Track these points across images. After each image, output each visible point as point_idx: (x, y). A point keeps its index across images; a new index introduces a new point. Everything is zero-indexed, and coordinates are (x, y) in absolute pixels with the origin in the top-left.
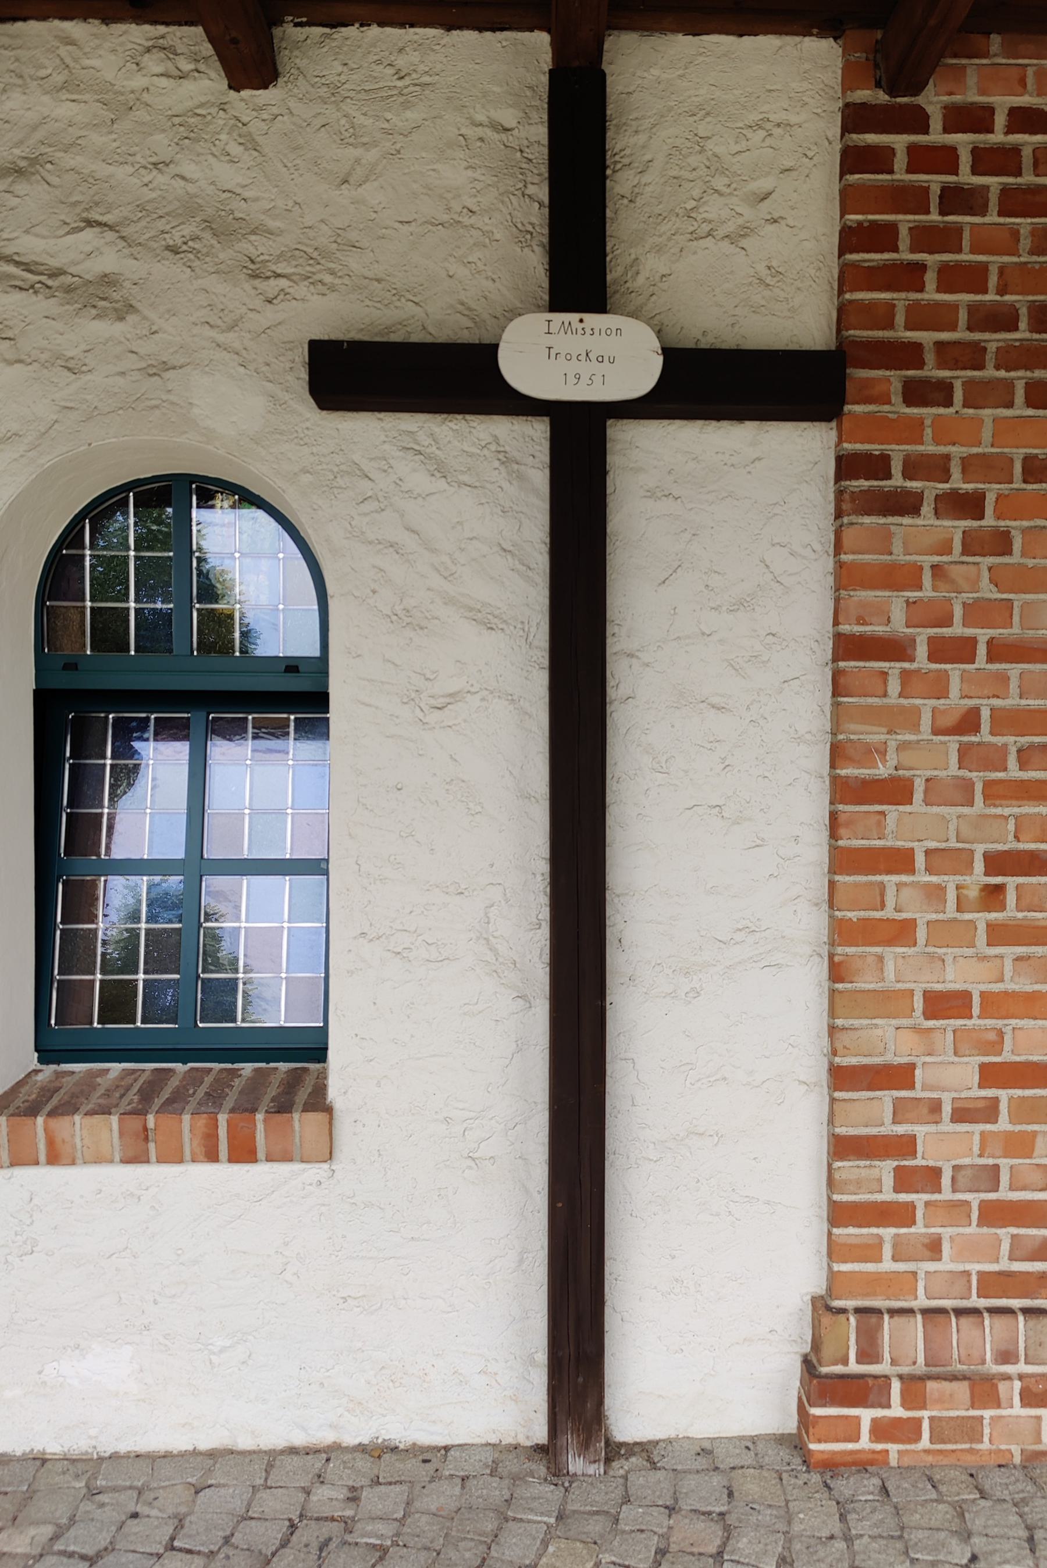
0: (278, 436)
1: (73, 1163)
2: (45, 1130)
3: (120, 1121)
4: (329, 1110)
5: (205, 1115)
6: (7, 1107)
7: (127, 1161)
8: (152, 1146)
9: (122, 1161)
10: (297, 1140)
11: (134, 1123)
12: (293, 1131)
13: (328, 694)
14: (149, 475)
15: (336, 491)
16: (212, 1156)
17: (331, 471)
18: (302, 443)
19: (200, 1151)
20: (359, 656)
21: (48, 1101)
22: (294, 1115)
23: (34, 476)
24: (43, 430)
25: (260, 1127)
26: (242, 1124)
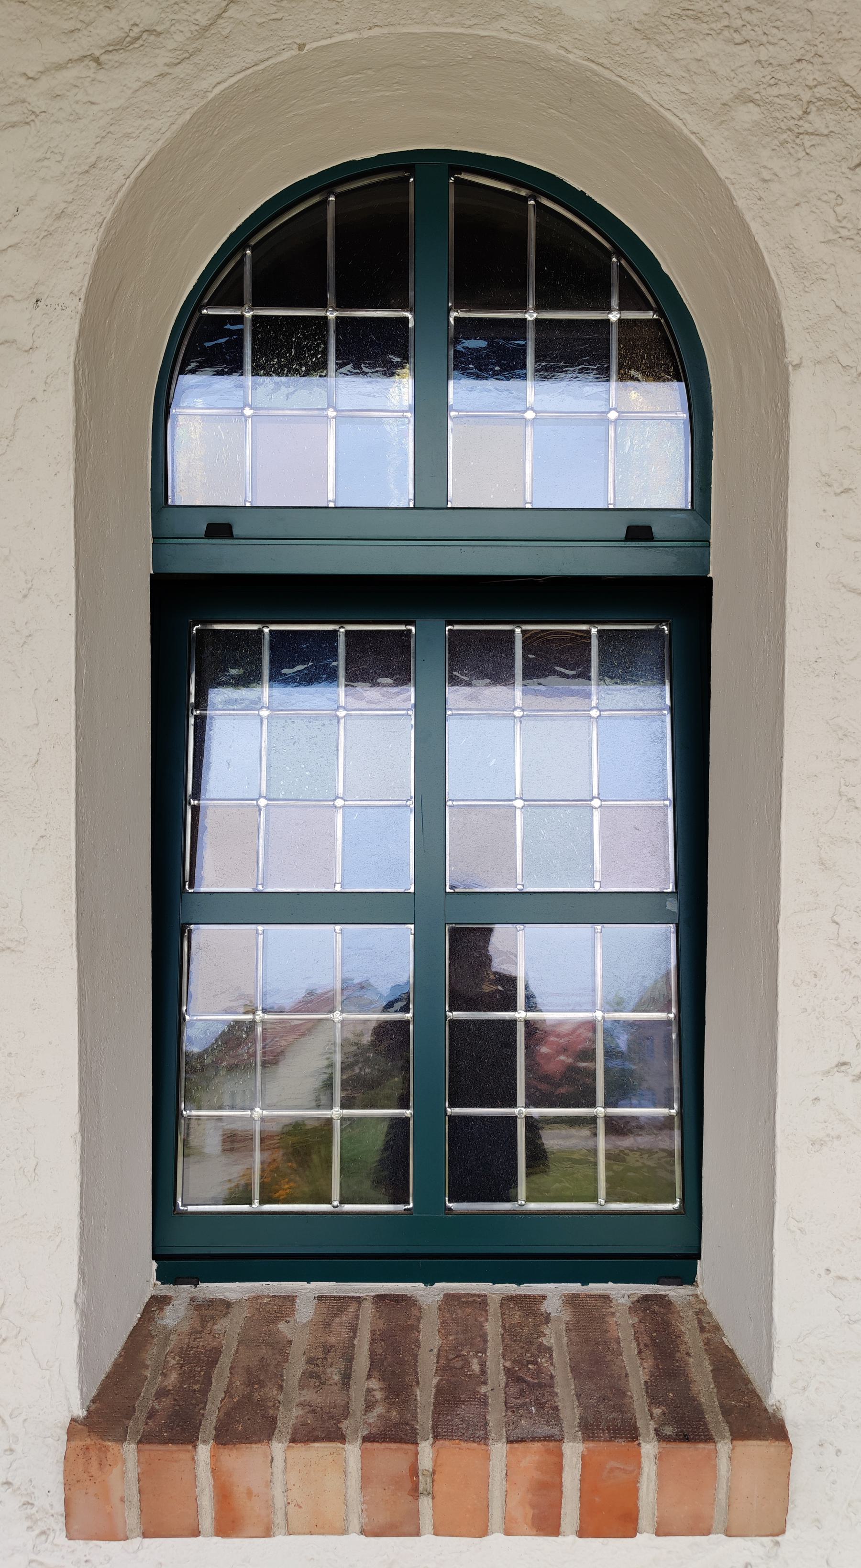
0: (689, 24)
1: (268, 1533)
2: (213, 1471)
3: (364, 1455)
4: (775, 1430)
5: (537, 1445)
6: (129, 1413)
7: (373, 1531)
8: (425, 1504)
9: (363, 1532)
10: (722, 1495)
11: (391, 1457)
12: (715, 1477)
13: (708, 583)
14: (373, 154)
15: (807, 141)
16: (547, 1524)
17: (797, 98)
18: (738, 38)
19: (522, 1513)
20: (847, 491)
21: (205, 1391)
22: (719, 1445)
23: (187, 116)
24: (204, 22)
25: (649, 1469)
26: (612, 1464)
